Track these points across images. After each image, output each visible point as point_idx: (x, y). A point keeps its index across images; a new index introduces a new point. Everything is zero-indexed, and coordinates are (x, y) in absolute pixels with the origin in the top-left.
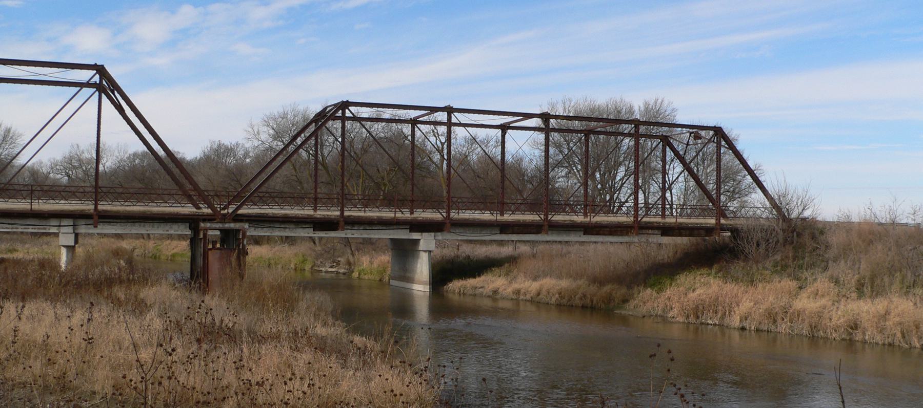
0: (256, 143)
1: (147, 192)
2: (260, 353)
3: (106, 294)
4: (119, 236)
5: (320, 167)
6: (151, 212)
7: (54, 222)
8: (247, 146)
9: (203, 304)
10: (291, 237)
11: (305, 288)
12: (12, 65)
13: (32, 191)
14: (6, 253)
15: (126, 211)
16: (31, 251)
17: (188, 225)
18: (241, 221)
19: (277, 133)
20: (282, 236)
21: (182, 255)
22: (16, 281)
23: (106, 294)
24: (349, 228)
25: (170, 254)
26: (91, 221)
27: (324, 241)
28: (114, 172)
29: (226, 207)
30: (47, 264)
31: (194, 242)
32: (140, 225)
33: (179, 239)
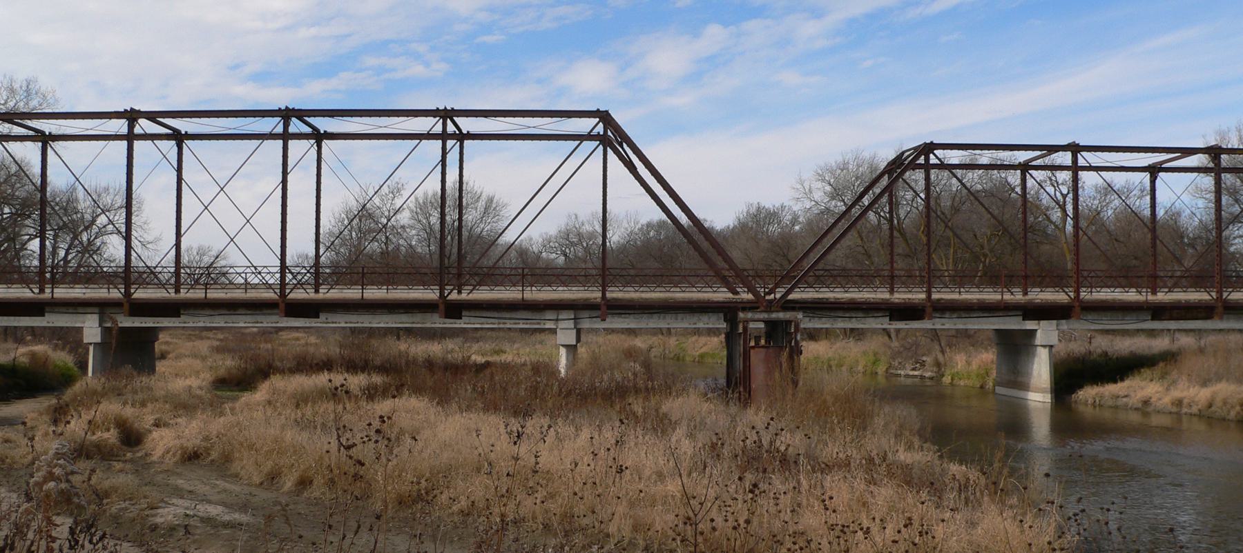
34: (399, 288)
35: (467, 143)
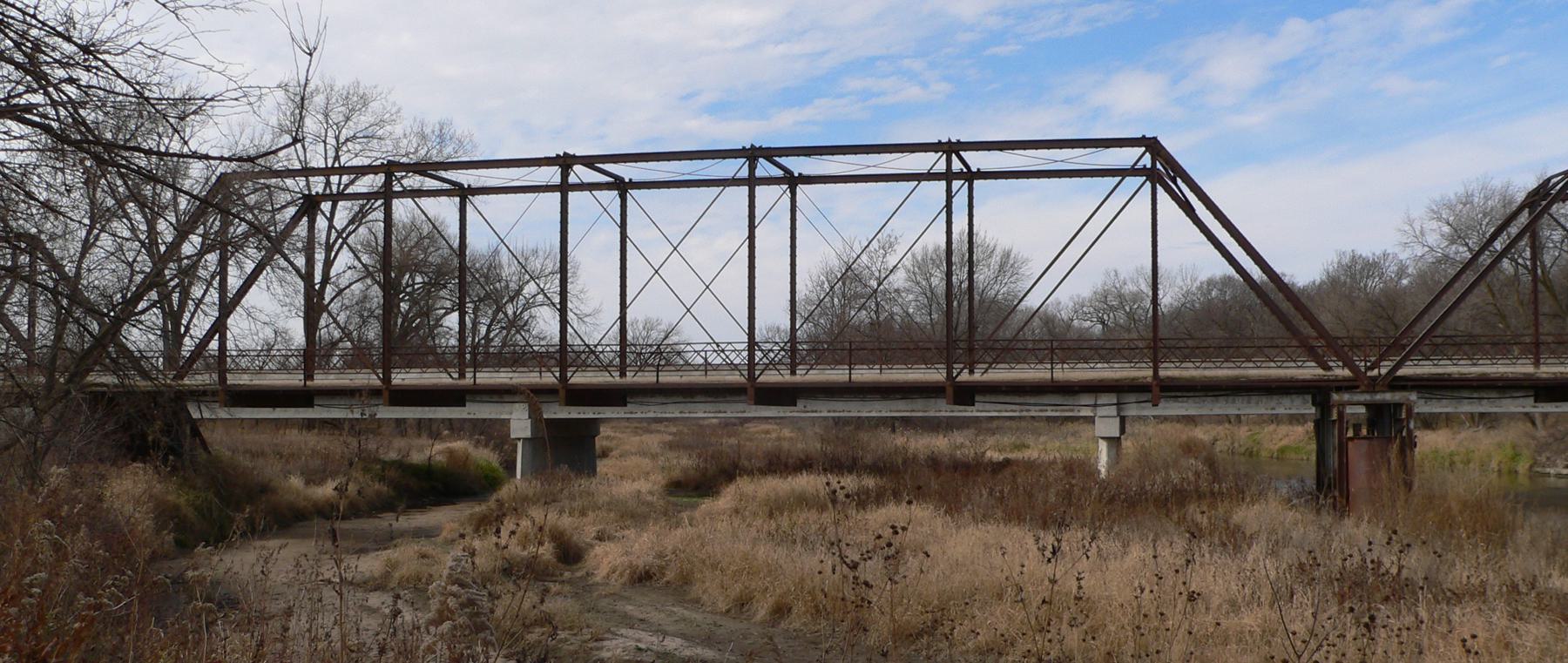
0: (1419, 251)
1: (1231, 348)
2: (1450, 622)
3: (1175, 517)
4: (1190, 420)
5: (1541, 287)
6: (1246, 377)
7: (1087, 399)
8: (1404, 255)
9: (1394, 537)
10: (1490, 413)
11: (1527, 506)
12: (821, 155)
13: (1052, 350)
14: (1011, 451)
15: (1205, 377)
16: (1049, 446)
17: (1309, 398)
18: (1404, 388)
19: (1456, 231)
20: (1472, 414)
21: (1297, 450)
22: (1030, 496)
23: (1175, 517)
24: (703, 400)
25: (1277, 447)
26: (1147, 396)
27: (1551, 420)
28: (1178, 313)
29: (1375, 365)
30: (1079, 469)
31: (1322, 426)
32: (1227, 402)
33: (1291, 423)
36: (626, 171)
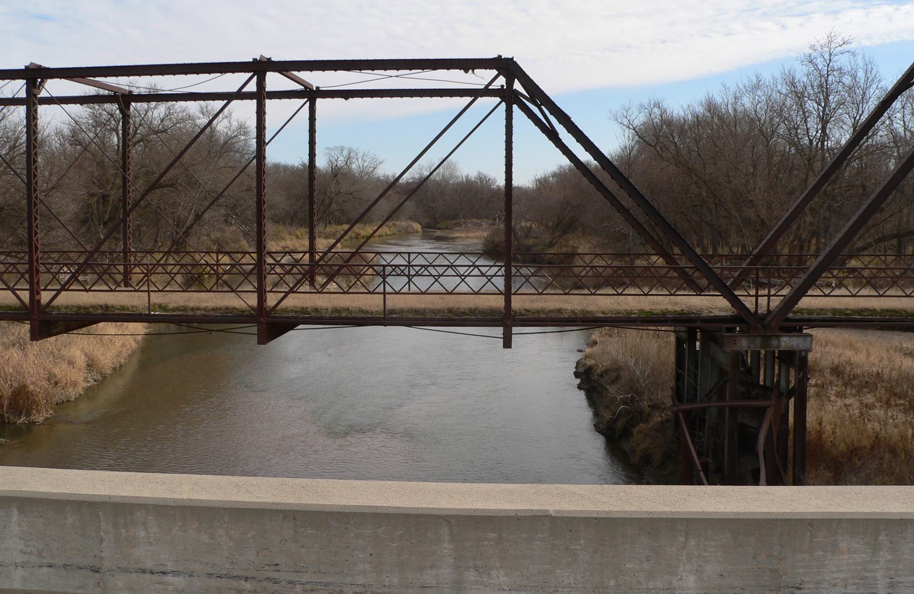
34: (653, 292)
35: (319, 102)
36: (317, 79)
